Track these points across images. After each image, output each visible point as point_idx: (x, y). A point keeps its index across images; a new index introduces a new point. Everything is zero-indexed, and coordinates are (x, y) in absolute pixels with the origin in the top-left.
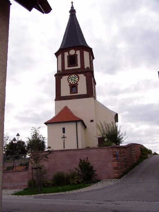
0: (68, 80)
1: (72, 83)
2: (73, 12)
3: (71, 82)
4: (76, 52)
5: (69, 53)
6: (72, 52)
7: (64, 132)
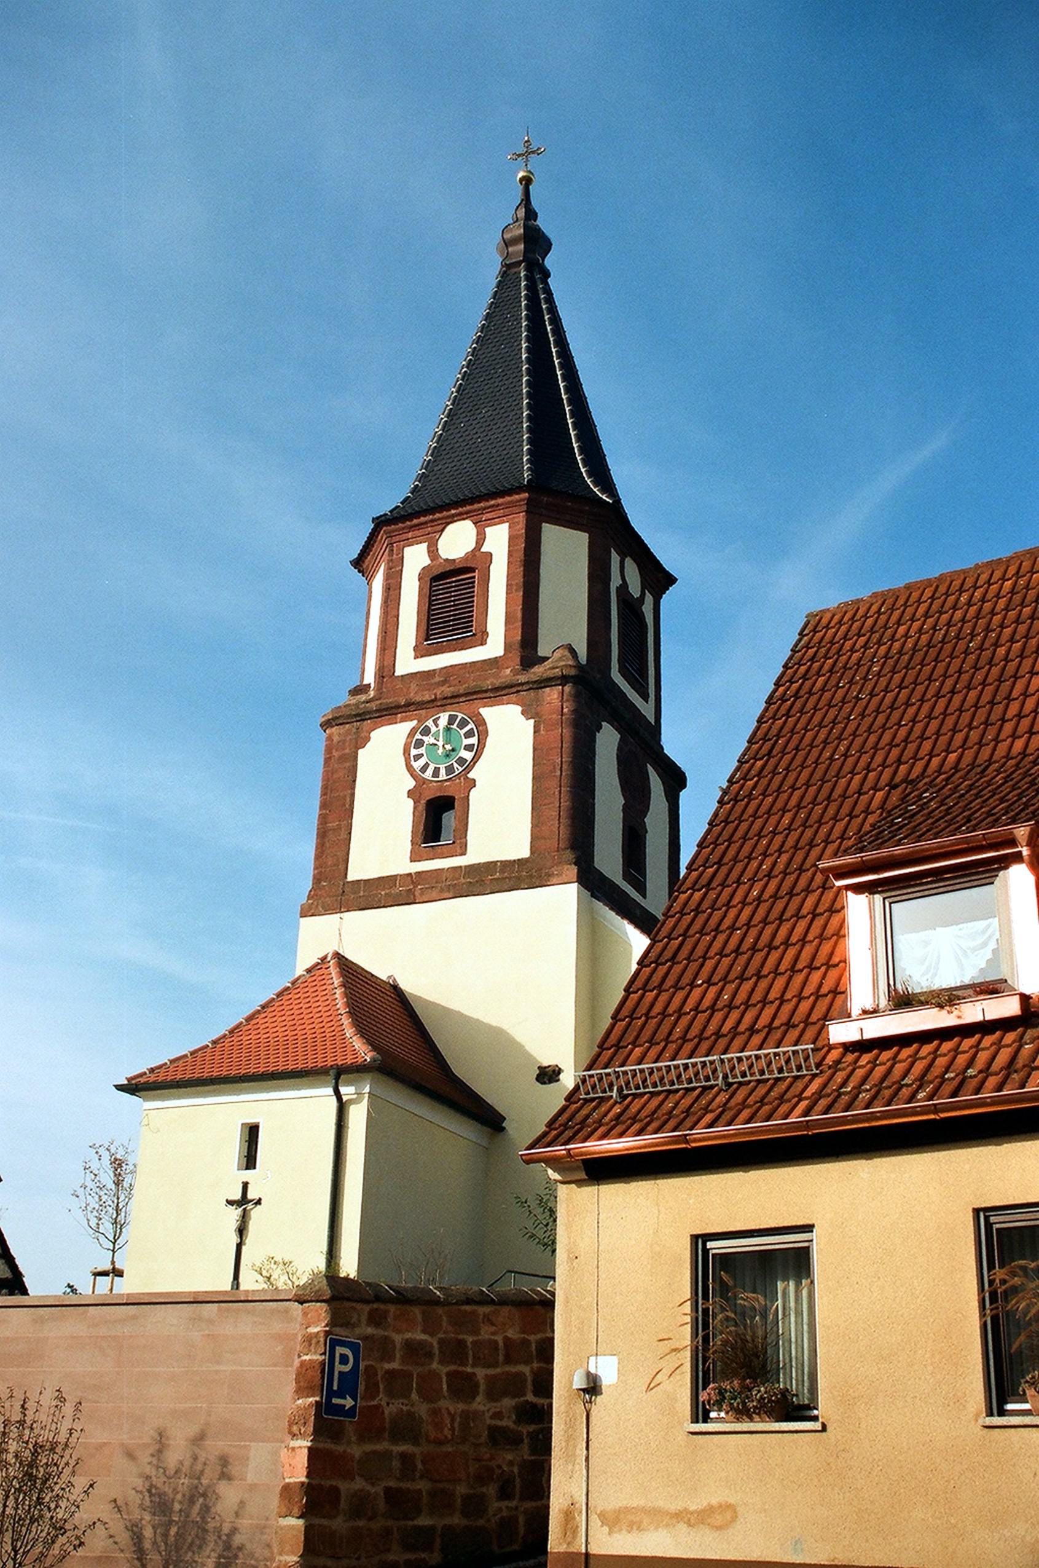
0: (406, 751)
1: (428, 774)
2: (532, 245)
3: (424, 768)
4: (481, 539)
5: (433, 552)
6: (457, 540)
7: (250, 1161)
